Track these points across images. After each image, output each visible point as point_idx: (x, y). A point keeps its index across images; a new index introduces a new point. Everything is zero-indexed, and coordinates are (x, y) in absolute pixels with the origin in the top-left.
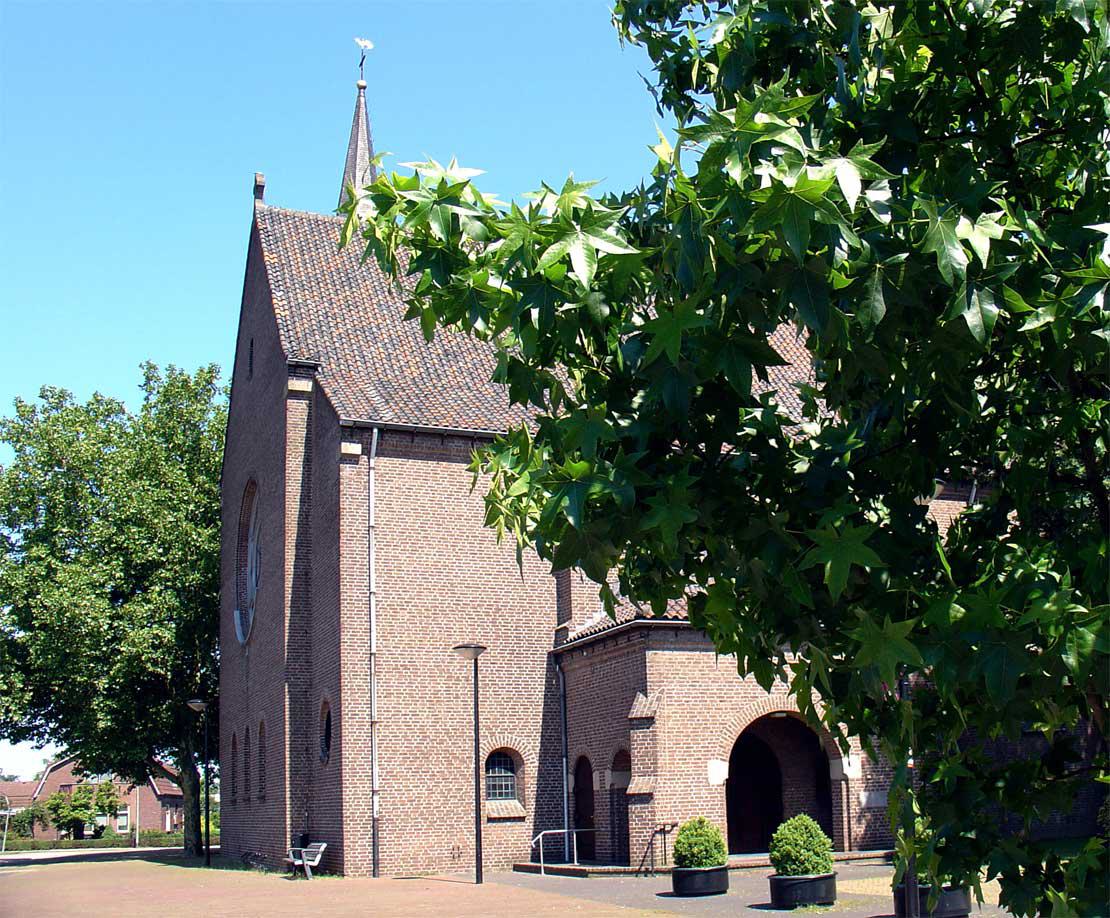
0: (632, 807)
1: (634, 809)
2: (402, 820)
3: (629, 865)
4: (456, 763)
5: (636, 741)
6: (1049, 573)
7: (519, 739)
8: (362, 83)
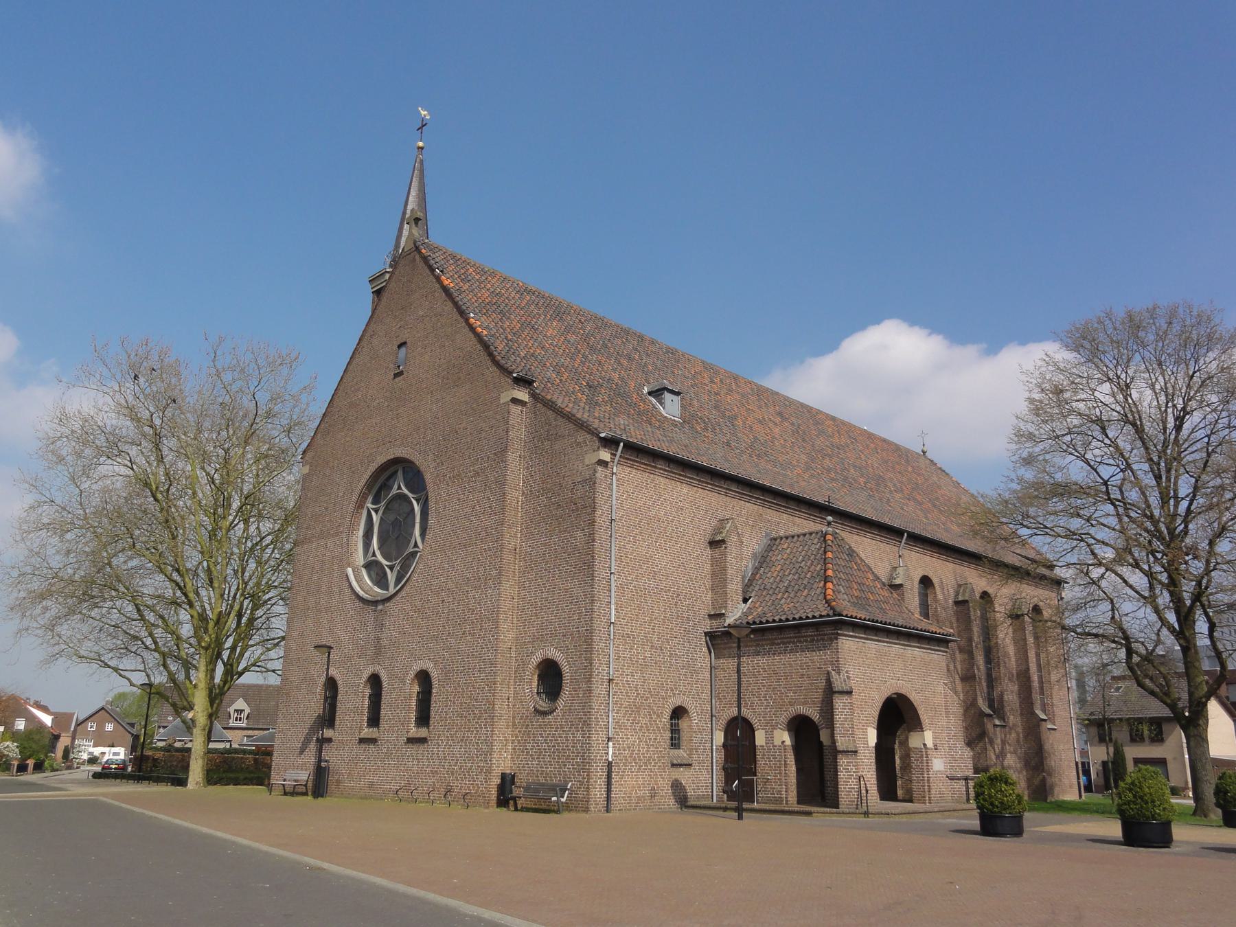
0: (840, 756)
1: (843, 761)
2: (623, 763)
3: (838, 808)
4: (654, 717)
5: (838, 709)
6: (371, 511)
7: (688, 699)
8: (421, 144)
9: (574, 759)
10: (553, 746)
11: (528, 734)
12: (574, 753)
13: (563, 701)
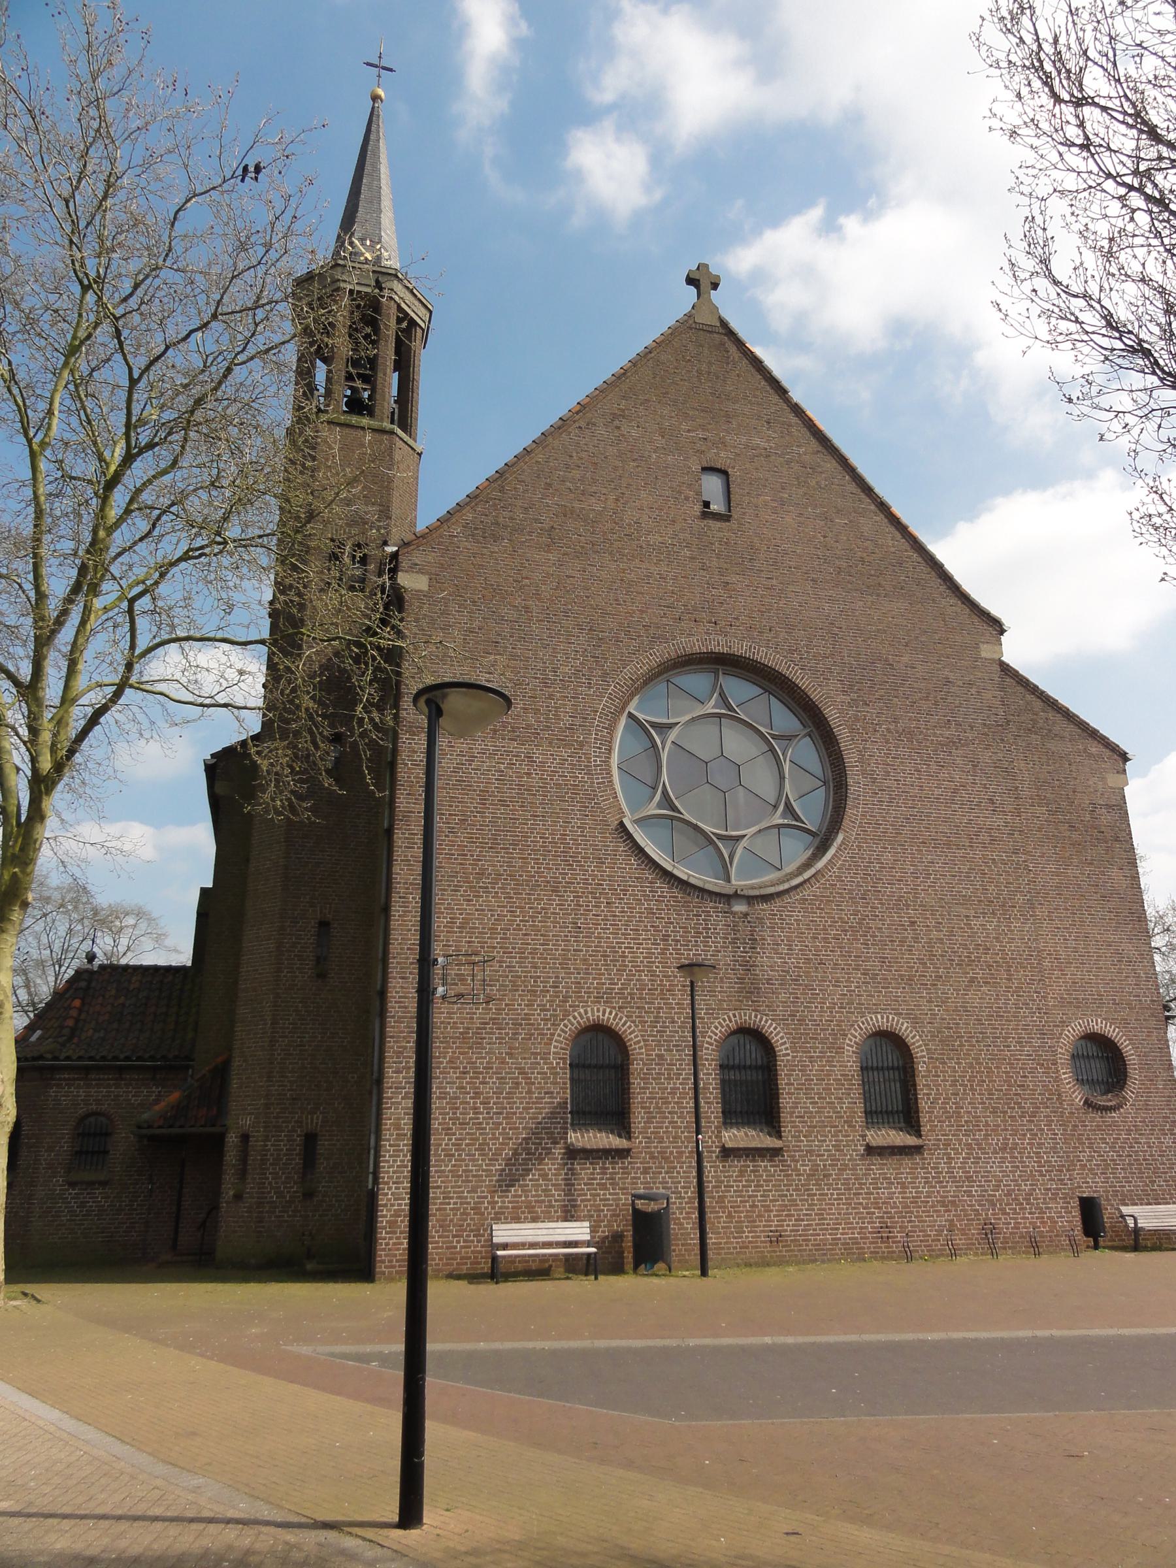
9: (1166, 1173)
10: (1127, 1156)
11: (1079, 1139)
12: (1164, 1164)
13: (1133, 1093)
